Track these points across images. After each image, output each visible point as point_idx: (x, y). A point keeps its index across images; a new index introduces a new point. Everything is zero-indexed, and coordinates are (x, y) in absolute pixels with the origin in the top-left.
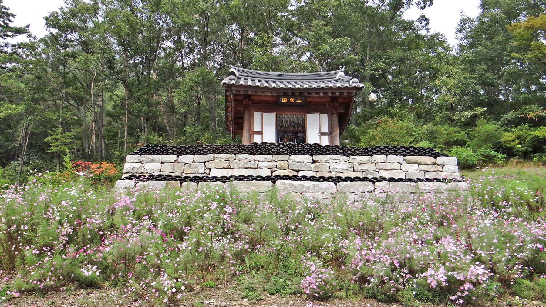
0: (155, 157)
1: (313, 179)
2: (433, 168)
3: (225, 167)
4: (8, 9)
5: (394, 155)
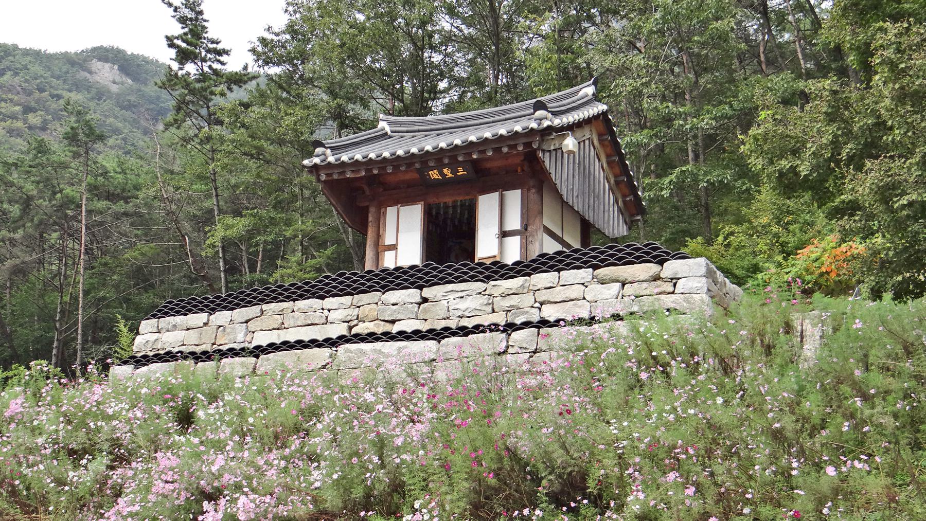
0: (179, 319)
1: (417, 335)
2: (653, 288)
3: (276, 326)
4: (217, 43)
5: (573, 268)
